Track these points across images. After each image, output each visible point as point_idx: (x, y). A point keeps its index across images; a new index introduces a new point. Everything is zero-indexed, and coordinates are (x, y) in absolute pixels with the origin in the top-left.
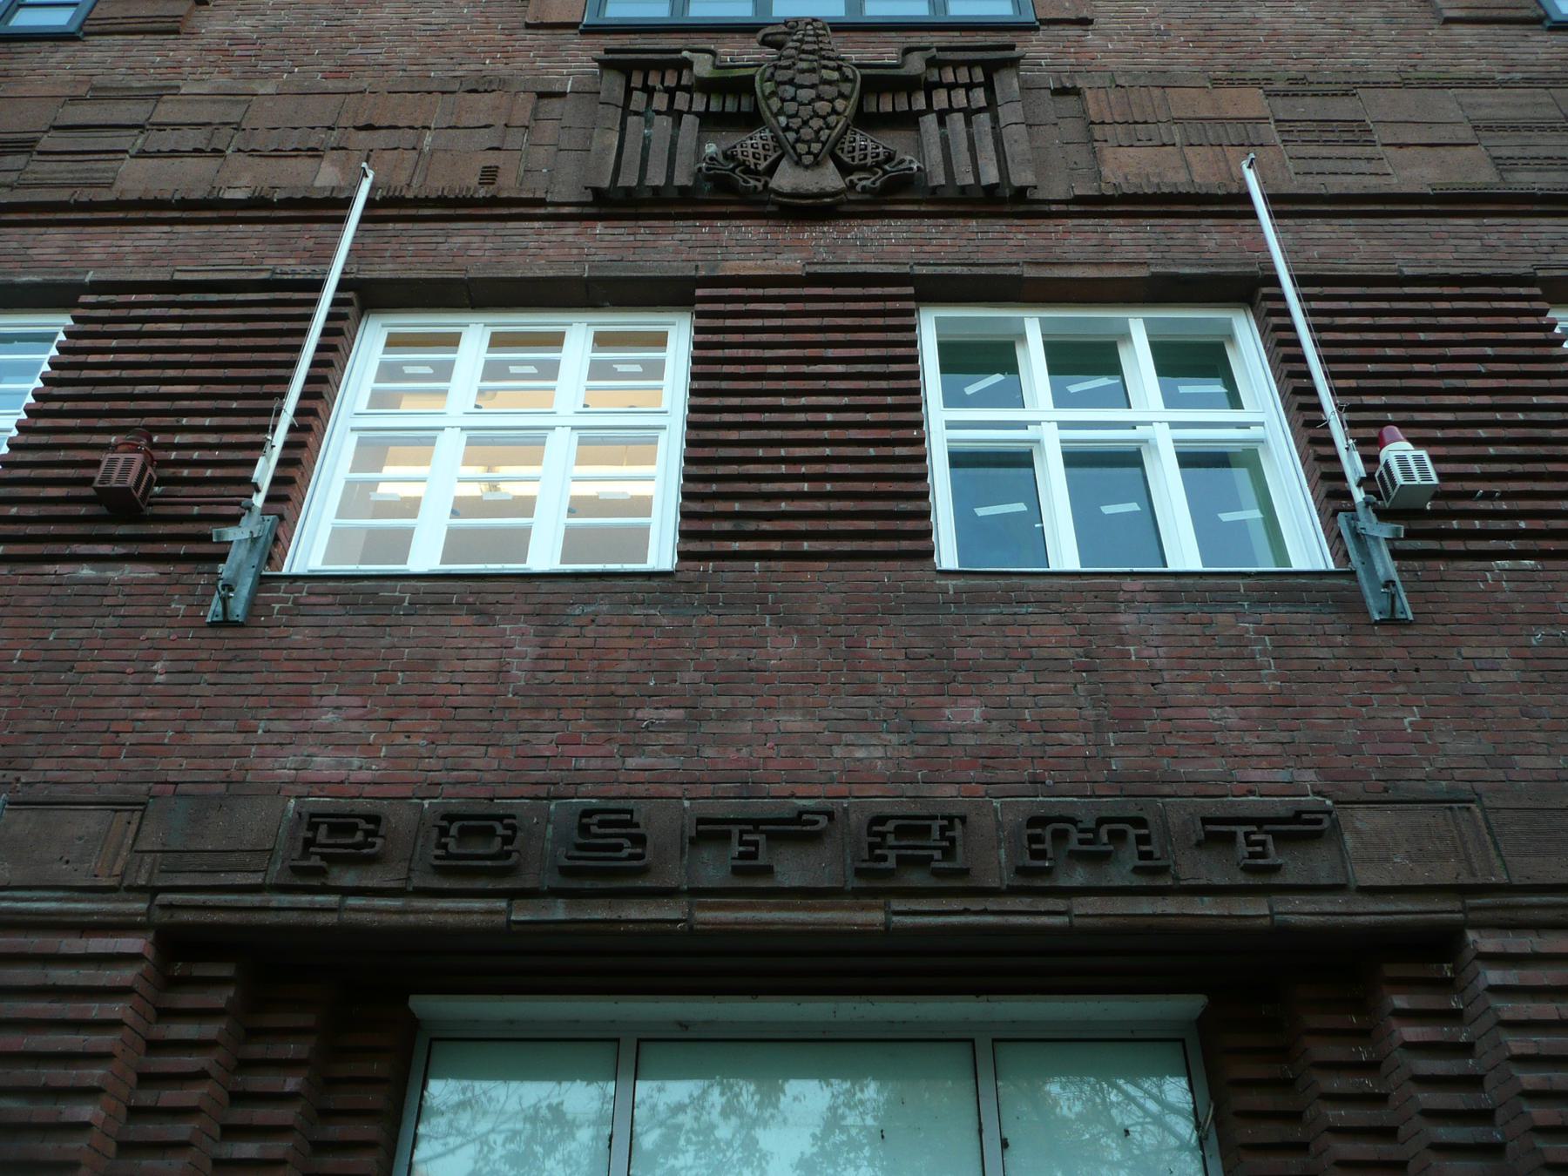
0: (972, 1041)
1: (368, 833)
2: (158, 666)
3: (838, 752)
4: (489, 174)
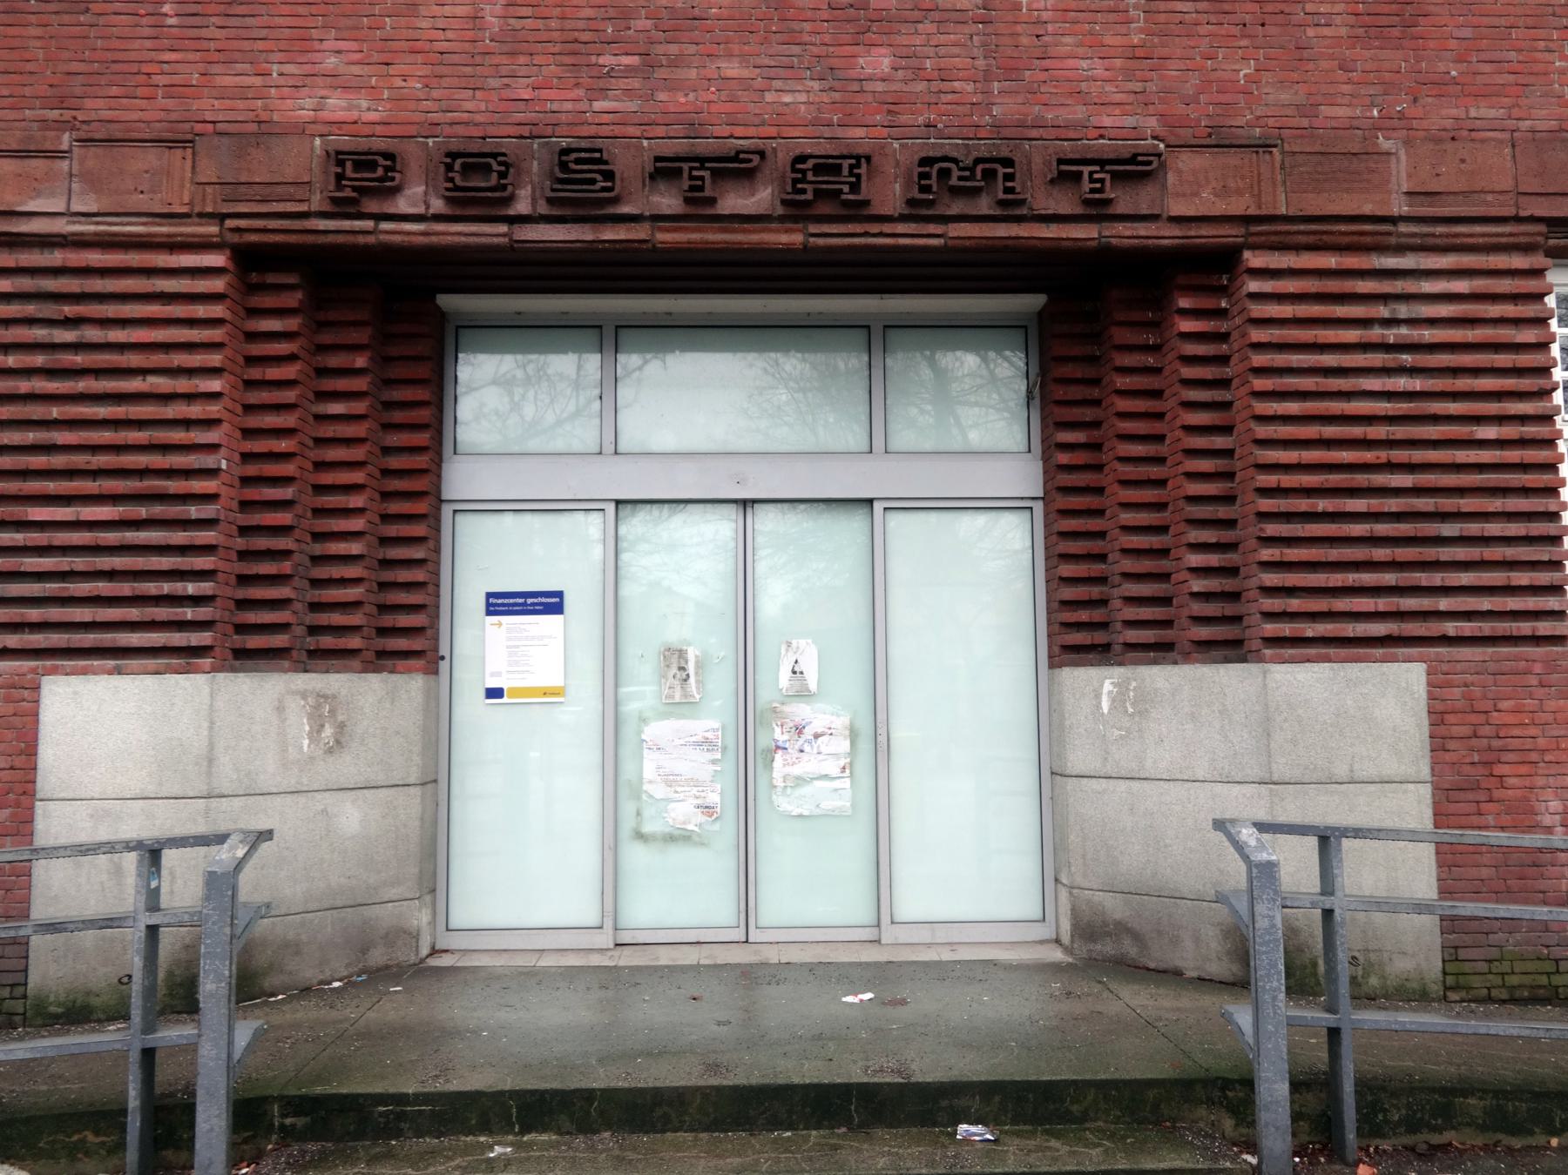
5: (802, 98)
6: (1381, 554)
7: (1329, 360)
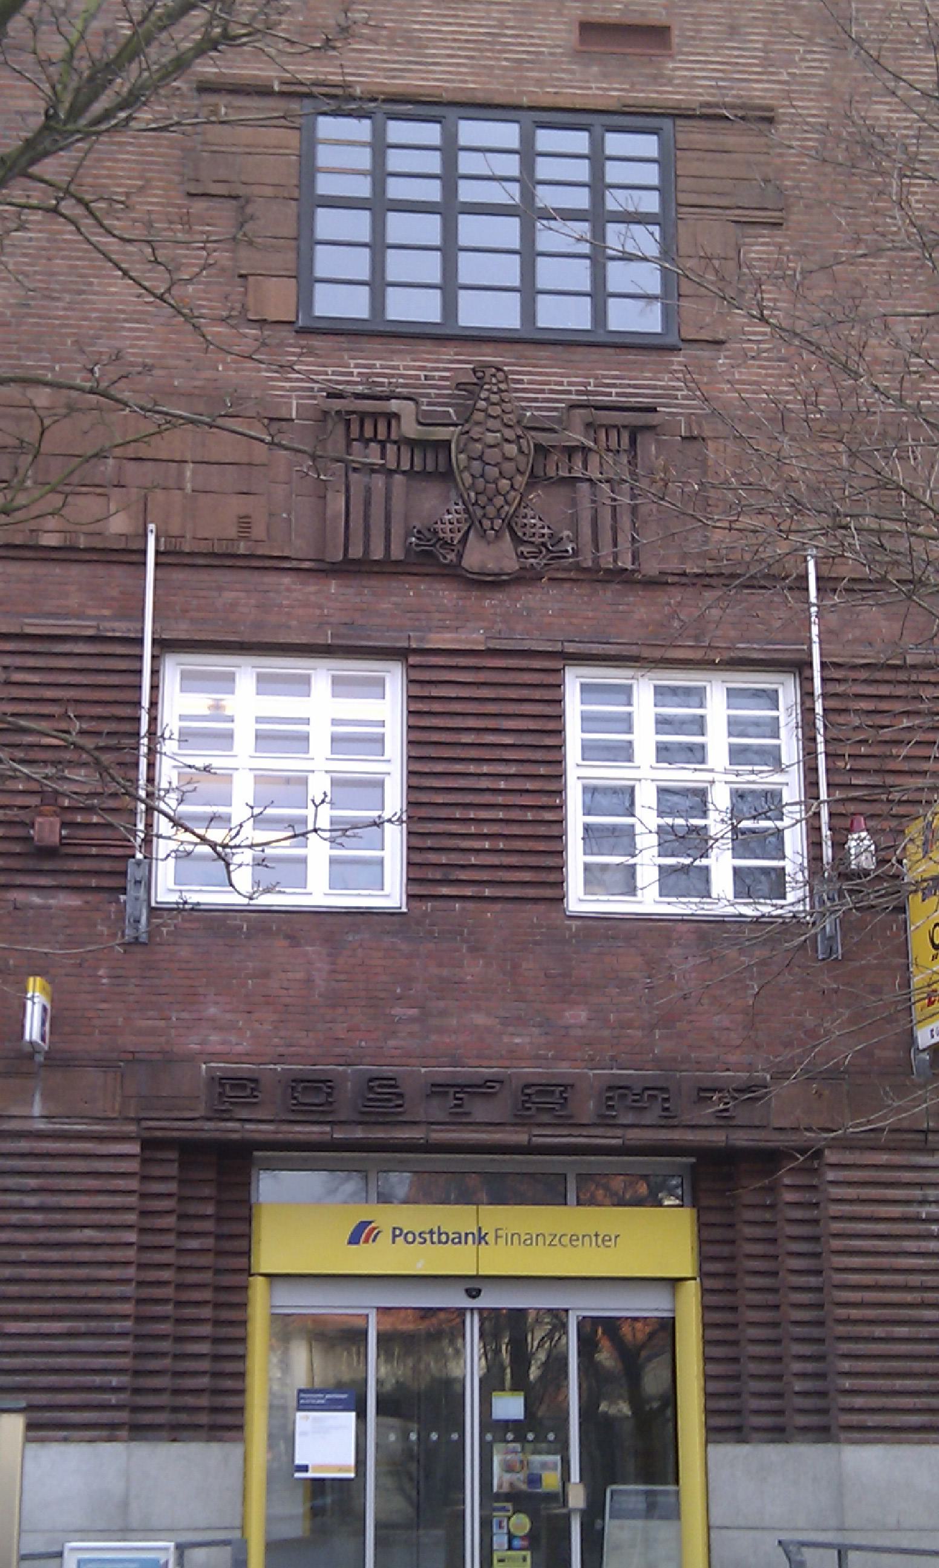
0: (565, 1175)
1: (253, 1089)
2: (101, 972)
3: (506, 1039)
4: (245, 523)
5: (527, 1040)
6: (917, 1366)
7: (881, 1228)
